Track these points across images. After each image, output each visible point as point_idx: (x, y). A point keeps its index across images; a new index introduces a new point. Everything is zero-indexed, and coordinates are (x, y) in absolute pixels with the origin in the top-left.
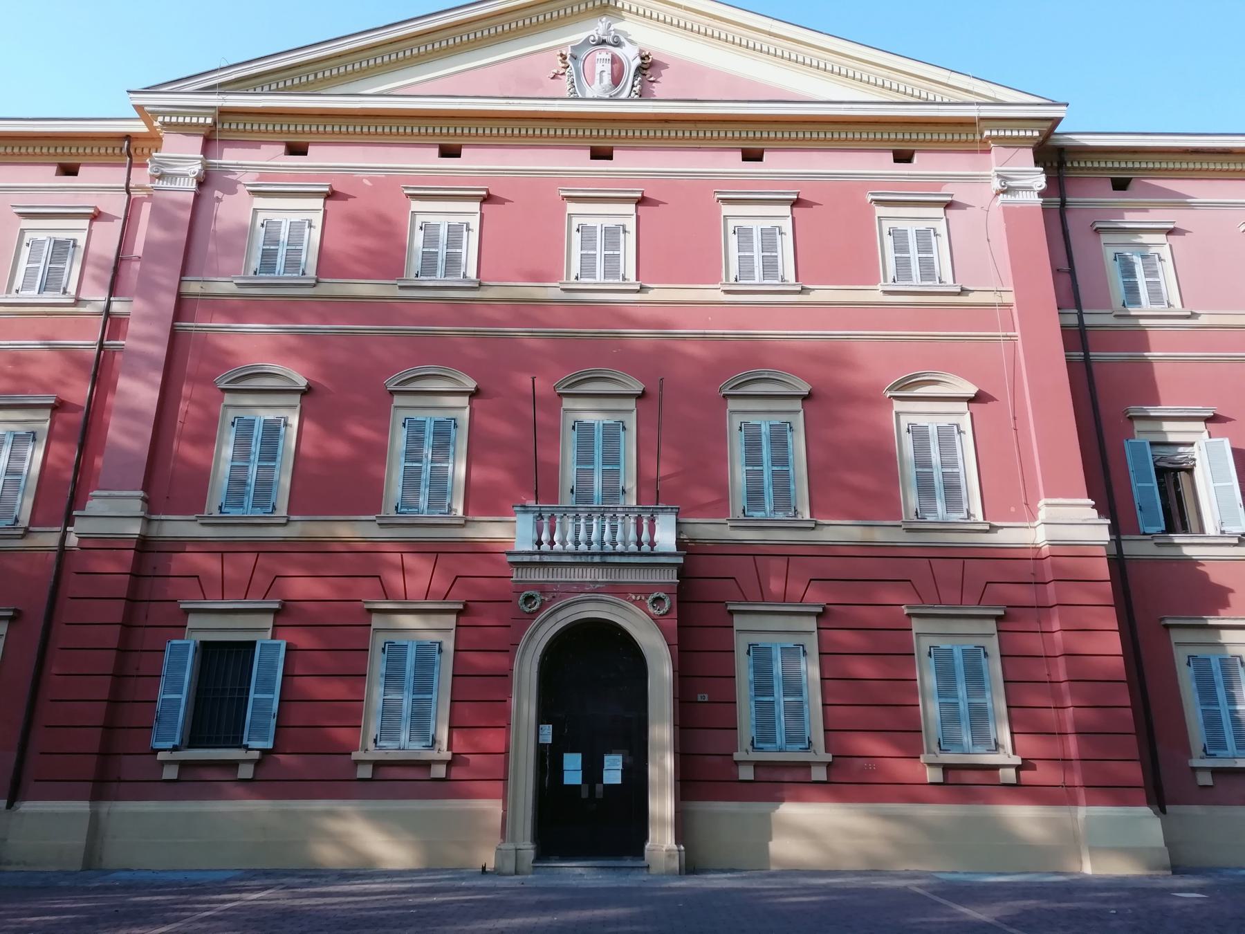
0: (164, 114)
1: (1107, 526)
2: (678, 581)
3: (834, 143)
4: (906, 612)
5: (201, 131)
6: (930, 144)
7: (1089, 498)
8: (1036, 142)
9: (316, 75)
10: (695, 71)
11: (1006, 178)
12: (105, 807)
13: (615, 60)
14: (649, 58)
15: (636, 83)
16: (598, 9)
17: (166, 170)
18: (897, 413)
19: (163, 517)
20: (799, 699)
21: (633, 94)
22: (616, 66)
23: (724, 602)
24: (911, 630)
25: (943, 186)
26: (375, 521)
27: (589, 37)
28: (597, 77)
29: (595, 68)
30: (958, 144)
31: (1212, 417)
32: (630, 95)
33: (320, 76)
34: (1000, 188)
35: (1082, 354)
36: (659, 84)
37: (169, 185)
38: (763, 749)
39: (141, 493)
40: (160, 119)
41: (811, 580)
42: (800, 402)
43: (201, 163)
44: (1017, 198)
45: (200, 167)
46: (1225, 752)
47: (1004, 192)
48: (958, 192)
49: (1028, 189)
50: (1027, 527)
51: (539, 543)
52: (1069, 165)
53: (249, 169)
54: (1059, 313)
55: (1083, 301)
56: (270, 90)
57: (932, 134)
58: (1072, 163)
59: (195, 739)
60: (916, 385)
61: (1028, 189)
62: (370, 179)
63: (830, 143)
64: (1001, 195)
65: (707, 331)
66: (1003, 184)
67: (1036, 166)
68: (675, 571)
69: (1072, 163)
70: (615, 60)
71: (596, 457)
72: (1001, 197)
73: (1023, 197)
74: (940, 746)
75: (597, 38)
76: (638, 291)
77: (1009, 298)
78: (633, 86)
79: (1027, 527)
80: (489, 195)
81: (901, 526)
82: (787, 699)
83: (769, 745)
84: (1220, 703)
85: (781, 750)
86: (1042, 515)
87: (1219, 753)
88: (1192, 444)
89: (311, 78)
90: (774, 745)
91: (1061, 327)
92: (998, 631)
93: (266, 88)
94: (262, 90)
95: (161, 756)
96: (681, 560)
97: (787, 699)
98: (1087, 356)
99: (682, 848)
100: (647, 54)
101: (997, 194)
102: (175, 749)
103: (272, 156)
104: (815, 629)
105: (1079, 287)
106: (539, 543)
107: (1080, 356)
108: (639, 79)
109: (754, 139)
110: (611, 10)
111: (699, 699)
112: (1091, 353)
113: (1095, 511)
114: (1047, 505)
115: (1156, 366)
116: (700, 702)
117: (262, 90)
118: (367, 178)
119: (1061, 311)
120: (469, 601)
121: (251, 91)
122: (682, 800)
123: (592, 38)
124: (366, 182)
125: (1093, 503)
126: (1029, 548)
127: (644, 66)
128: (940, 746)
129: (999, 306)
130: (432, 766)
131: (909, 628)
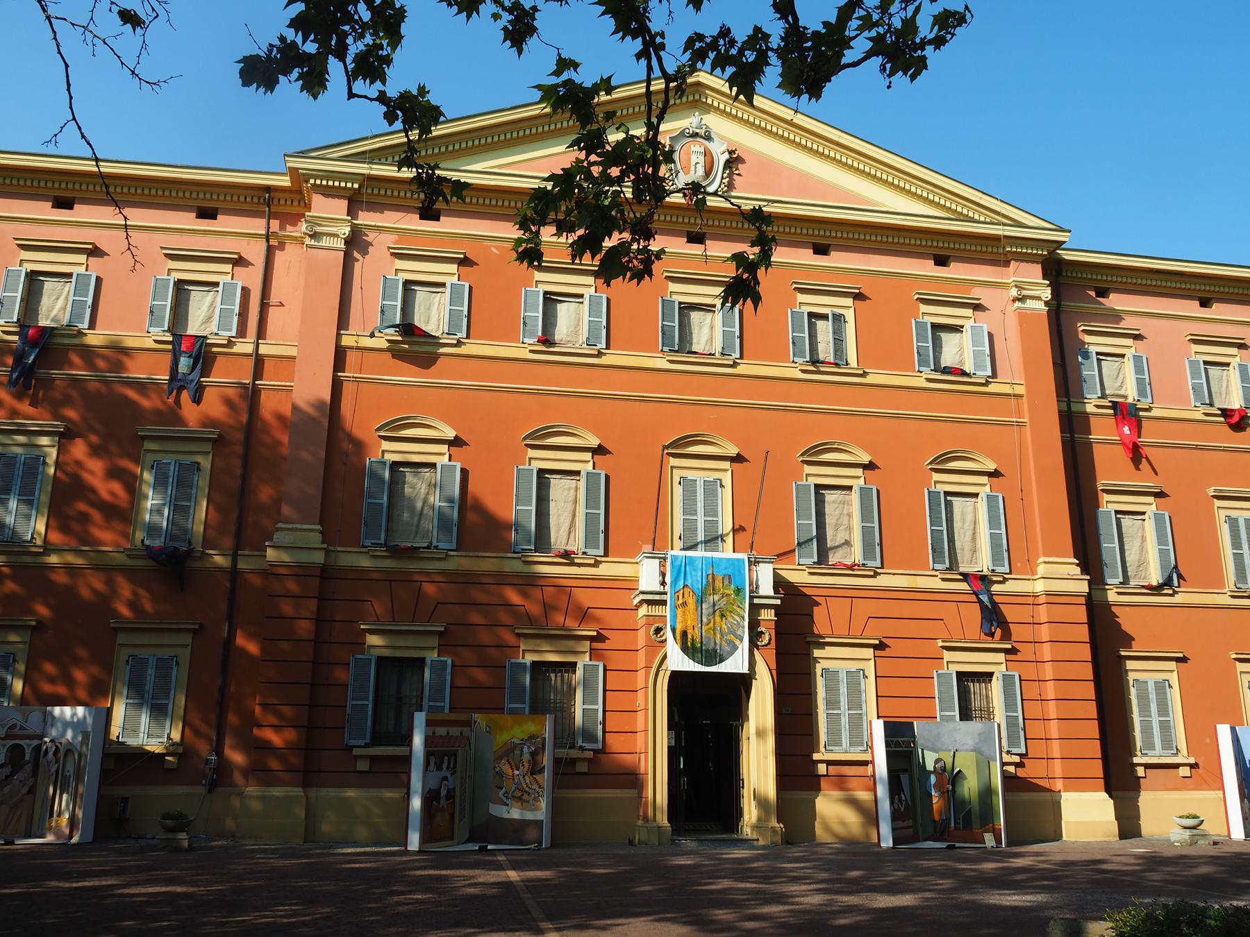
0: (315, 178)
1: (1087, 581)
2: (776, 619)
3: (672, 224)
4: (941, 644)
5: (346, 193)
6: (985, 254)
7: (1075, 558)
8: (1044, 258)
9: (447, 148)
10: (770, 167)
11: (1020, 287)
12: (313, 792)
13: (707, 153)
14: (735, 153)
15: (725, 175)
16: (690, 102)
17: (318, 229)
18: (672, 467)
19: (339, 549)
20: (860, 712)
21: (723, 186)
22: (708, 158)
23: (512, 626)
24: (943, 659)
25: (971, 289)
26: (520, 558)
27: (685, 129)
28: (693, 168)
29: (690, 158)
30: (979, 254)
31: (1159, 492)
32: (720, 187)
33: (451, 148)
34: (1017, 295)
35: (1069, 435)
36: (741, 177)
37: (316, 243)
38: (832, 750)
39: (318, 527)
40: (312, 181)
41: (869, 617)
42: (590, 454)
43: (351, 226)
44: (1025, 306)
45: (349, 229)
46: (1154, 752)
47: (1019, 300)
48: (978, 294)
49: (1038, 298)
50: (1029, 580)
51: (663, 583)
52: (1064, 274)
53: (383, 230)
54: (1058, 401)
55: (1071, 393)
56: (393, 161)
57: (853, 233)
58: (1066, 273)
59: (376, 740)
60: (402, 428)
61: (1038, 298)
62: (497, 248)
63: (680, 225)
64: (1017, 302)
65: (788, 404)
66: (1019, 293)
67: (1044, 279)
68: (773, 611)
69: (1066, 273)
70: (707, 153)
71: (699, 509)
72: (1017, 304)
73: (1030, 304)
74: (825, 748)
75: (691, 132)
76: (730, 366)
77: (1020, 390)
78: (722, 178)
79: (1029, 580)
80: (466, 257)
81: (937, 576)
82: (850, 712)
83: (837, 748)
84: (1153, 715)
85: (846, 752)
86: (1041, 570)
87: (1150, 753)
88: (1144, 513)
89: (443, 149)
90: (841, 748)
91: (1059, 412)
92: (1006, 661)
93: (390, 159)
94: (386, 160)
95: (356, 752)
96: (778, 602)
97: (850, 712)
98: (1072, 437)
99: (782, 826)
100: (734, 149)
101: (1014, 301)
102: (366, 746)
103: (805, 257)
104: (1004, 661)
105: (1069, 379)
106: (663, 583)
107: (1068, 437)
108: (727, 172)
109: (824, 236)
110: (701, 105)
111: (784, 712)
112: (1076, 436)
113: (1079, 569)
114: (1045, 563)
115: (1097, 449)
116: (784, 714)
117: (386, 160)
118: (495, 247)
119: (1060, 399)
120: (450, 624)
121: (383, 161)
122: (1007, 791)
123: (687, 131)
124: (494, 250)
125: (1077, 562)
126: (1030, 596)
127: (731, 160)
128: (825, 748)
129: (356, 349)
130: (577, 764)
131: (941, 657)
